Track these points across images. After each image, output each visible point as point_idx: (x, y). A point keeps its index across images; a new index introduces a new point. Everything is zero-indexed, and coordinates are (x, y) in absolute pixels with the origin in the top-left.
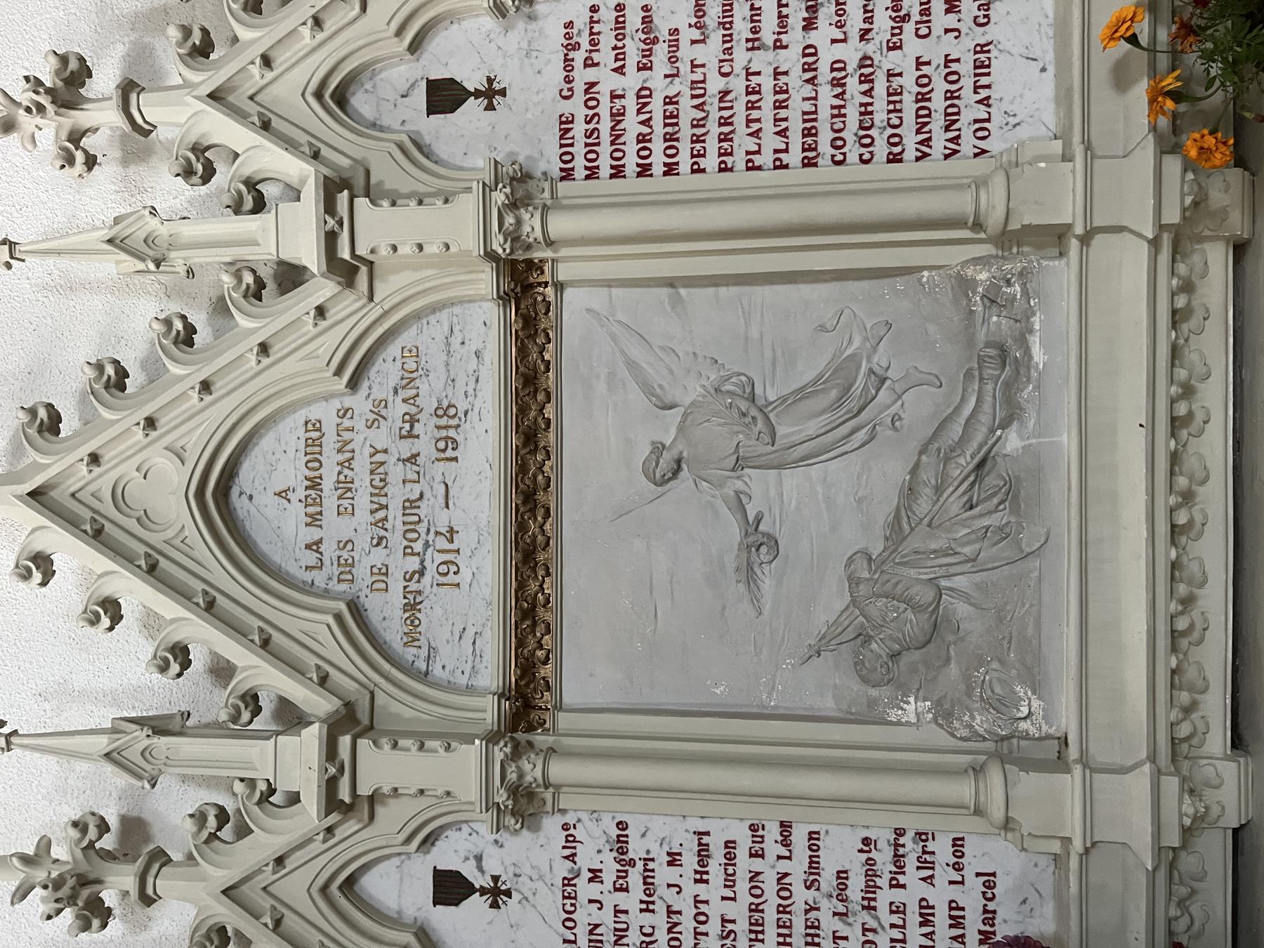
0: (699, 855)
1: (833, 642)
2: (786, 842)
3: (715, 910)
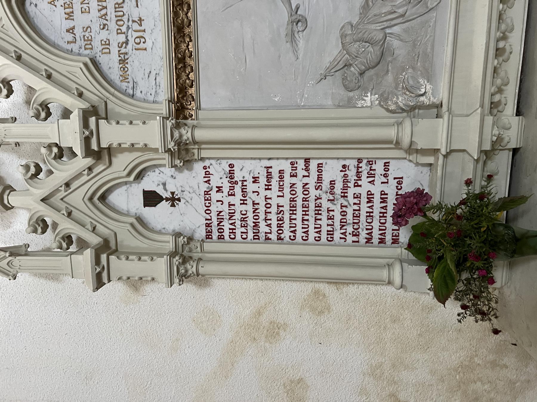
0: (267, 178)
1: (333, 71)
2: (307, 169)
3: (274, 202)
